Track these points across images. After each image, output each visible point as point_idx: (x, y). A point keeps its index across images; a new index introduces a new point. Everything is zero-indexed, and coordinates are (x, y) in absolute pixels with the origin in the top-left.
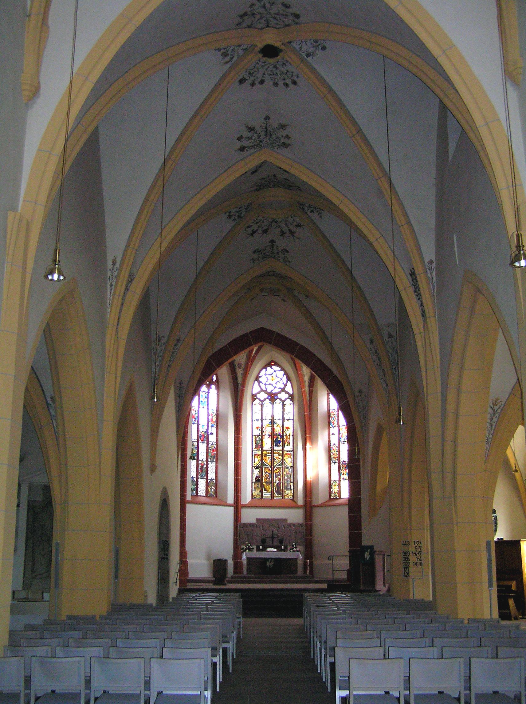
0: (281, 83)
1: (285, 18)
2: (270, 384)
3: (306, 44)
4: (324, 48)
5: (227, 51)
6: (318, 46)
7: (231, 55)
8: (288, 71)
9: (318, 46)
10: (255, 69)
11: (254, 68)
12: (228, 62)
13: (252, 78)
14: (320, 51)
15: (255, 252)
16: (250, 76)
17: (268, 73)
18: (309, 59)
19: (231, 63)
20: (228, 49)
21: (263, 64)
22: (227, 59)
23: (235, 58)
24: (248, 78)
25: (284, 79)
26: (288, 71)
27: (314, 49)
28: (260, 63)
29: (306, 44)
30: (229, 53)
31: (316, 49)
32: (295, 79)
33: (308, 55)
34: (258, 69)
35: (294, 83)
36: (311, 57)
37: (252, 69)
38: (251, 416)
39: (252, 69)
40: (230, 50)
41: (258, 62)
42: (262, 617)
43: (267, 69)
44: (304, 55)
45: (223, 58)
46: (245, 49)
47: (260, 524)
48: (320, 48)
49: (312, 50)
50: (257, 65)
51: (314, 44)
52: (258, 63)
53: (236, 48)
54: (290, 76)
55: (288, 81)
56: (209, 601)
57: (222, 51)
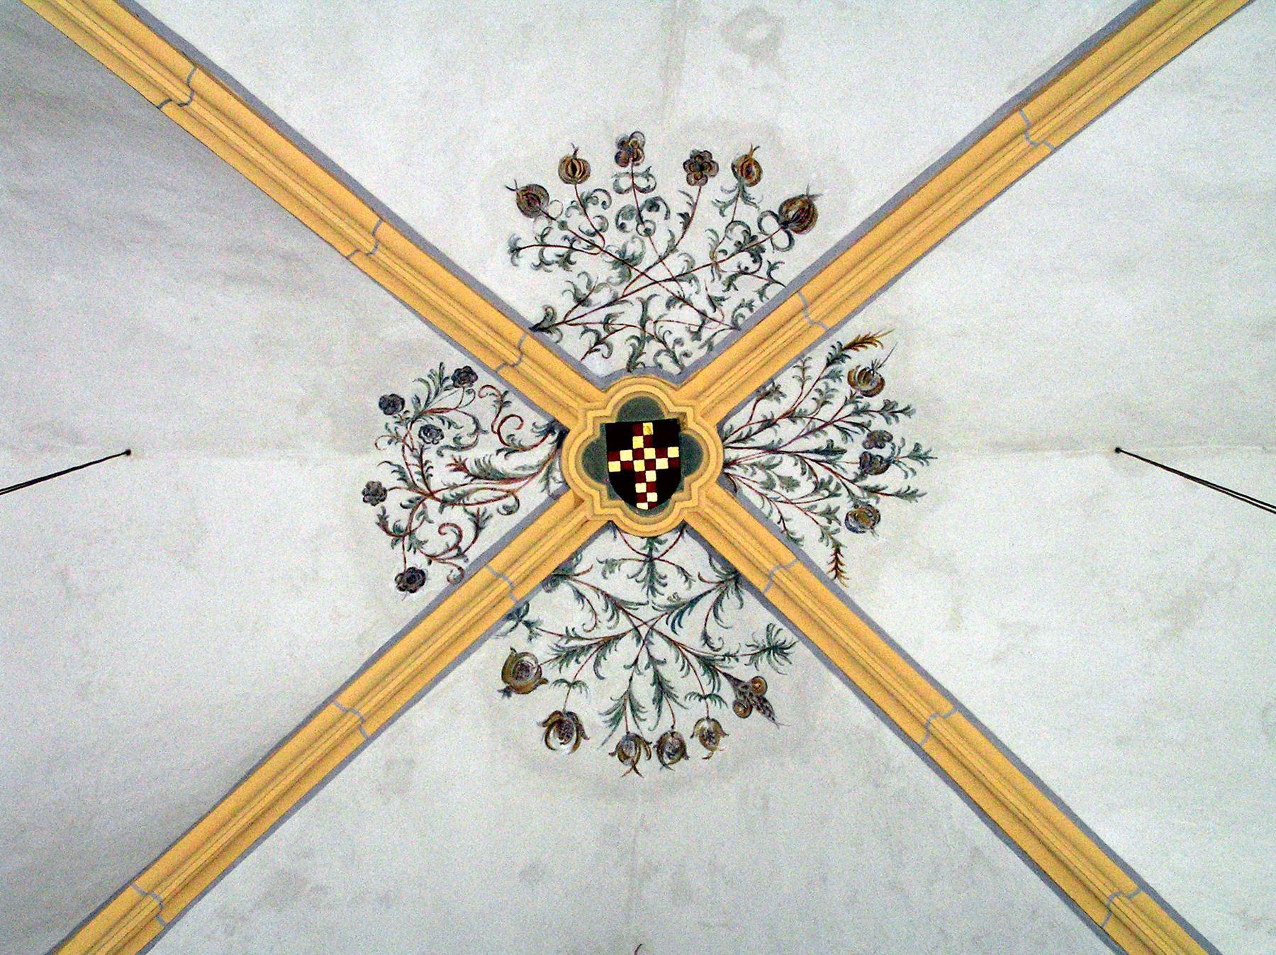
0: (603, 170)
3: (476, 422)
4: (391, 404)
5: (851, 400)
7: (835, 376)
8: (566, 262)
9: (419, 415)
10: (729, 267)
13: (748, 214)
14: (407, 396)
15: (882, 380)
16: (755, 231)
18: (455, 361)
19: (847, 335)
22: (860, 359)
23: (817, 363)
25: (583, 203)
26: (566, 262)
29: (476, 422)
30: (843, 389)
31: (427, 404)
32: (528, 229)
33: (464, 377)
35: (531, 200)
36: (449, 372)
39: (744, 272)
43: (672, 249)
44: (484, 378)
45: (875, 366)
46: (767, 395)
48: (409, 406)
49: (450, 398)
50: (717, 290)
51: (436, 422)
53: (809, 405)
55: (561, 195)
56: (149, 82)
57: (876, 402)
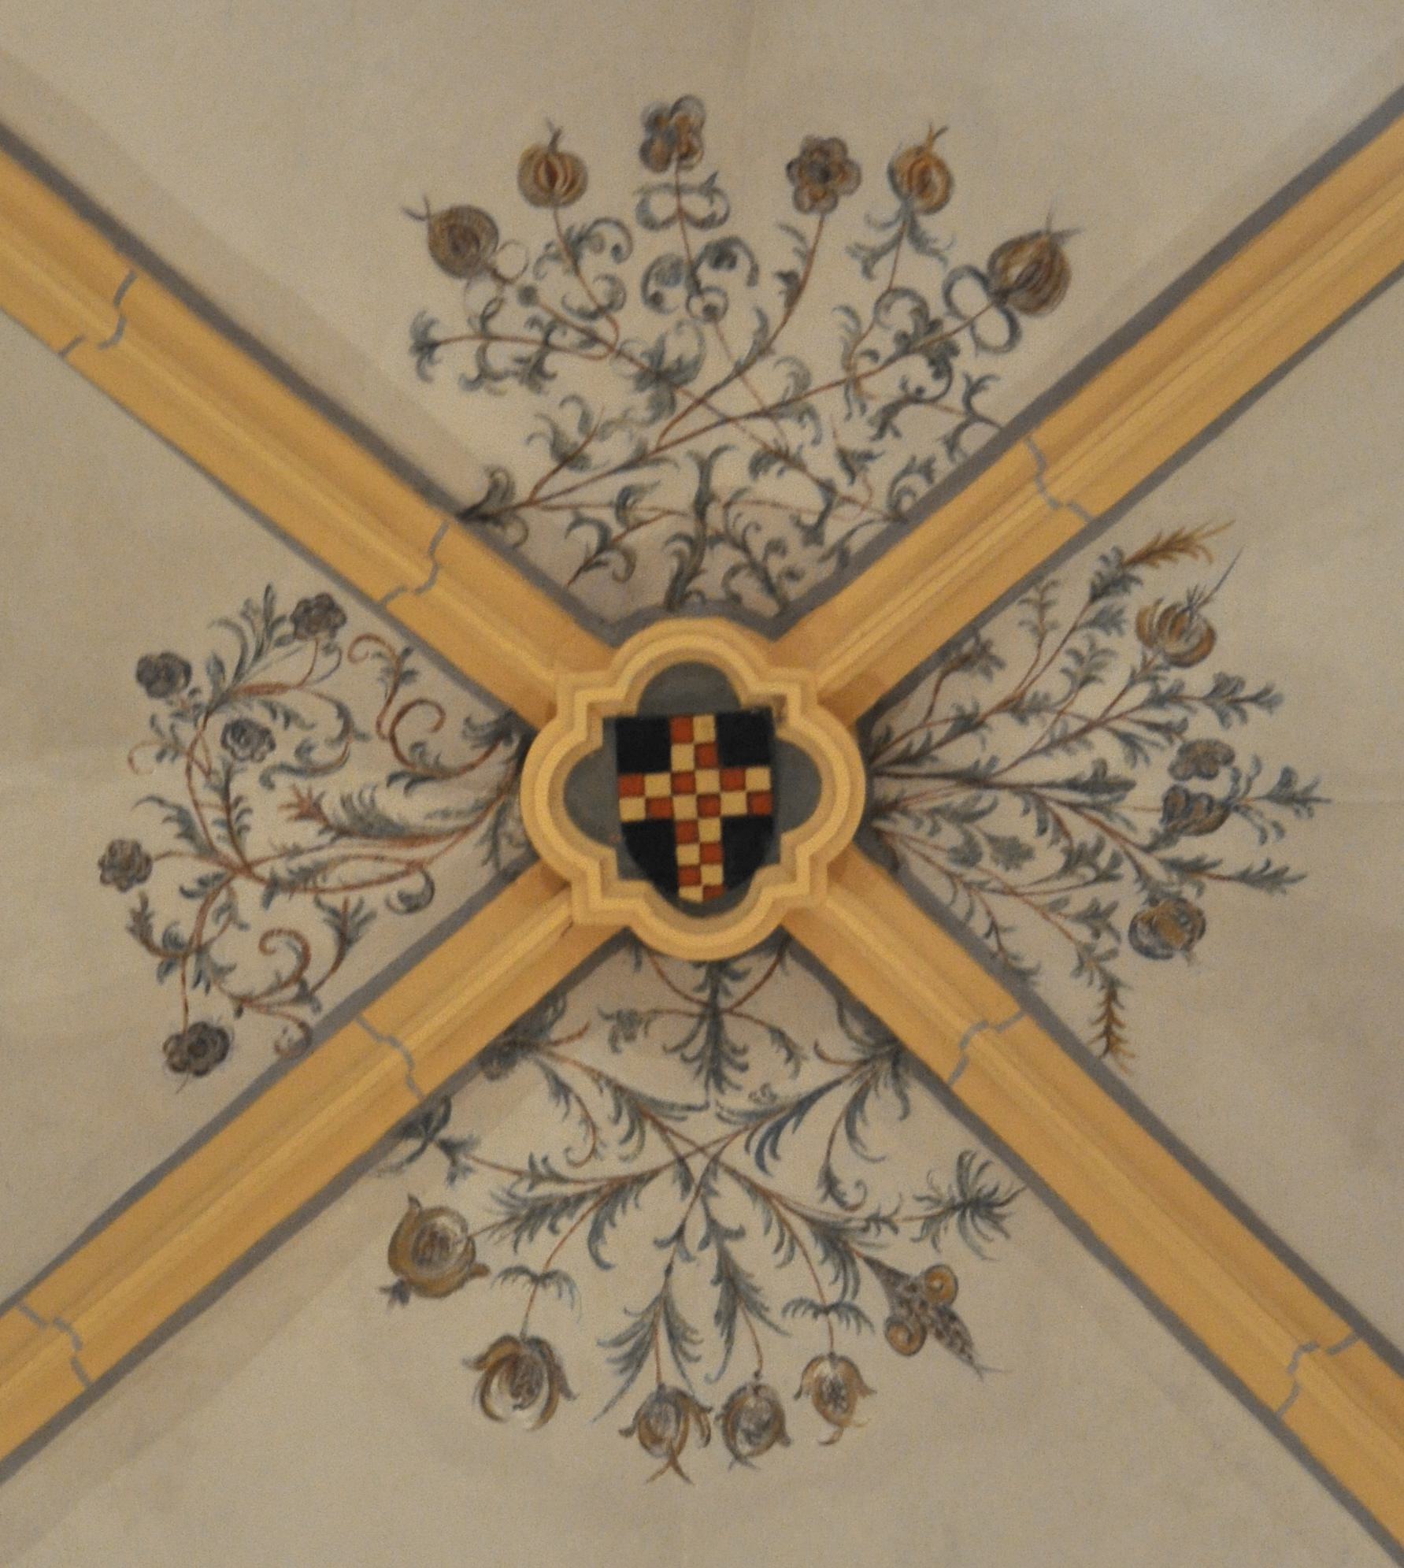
1: (537, 1173)
2: (338, 665)
3: (343, 712)
5: (1144, 674)
6: (222, 700)
8: (534, 373)
9: (222, 700)
10: (883, 387)
11: (890, 411)
12: (1149, 555)
14: (197, 656)
17: (753, 279)
20: (1142, 692)
21: (793, 434)
24: (971, 296)
26: (534, 373)
27: (257, 676)
28: (822, 462)
29: (343, 712)
30: (1127, 650)
31: (239, 673)
34: (852, 383)
36: (285, 605)
37: (916, 397)
38: (1338, 338)
39: (916, 397)
40: (1116, 676)
41: (841, 481)
42: (964, 488)
43: (762, 348)
45: (1194, 602)
47: (1133, 603)
48: (200, 678)
50: (857, 435)
51: (259, 715)
52: (852, 474)
53: (1054, 684)
54: (512, 318)
57: (1198, 679)
